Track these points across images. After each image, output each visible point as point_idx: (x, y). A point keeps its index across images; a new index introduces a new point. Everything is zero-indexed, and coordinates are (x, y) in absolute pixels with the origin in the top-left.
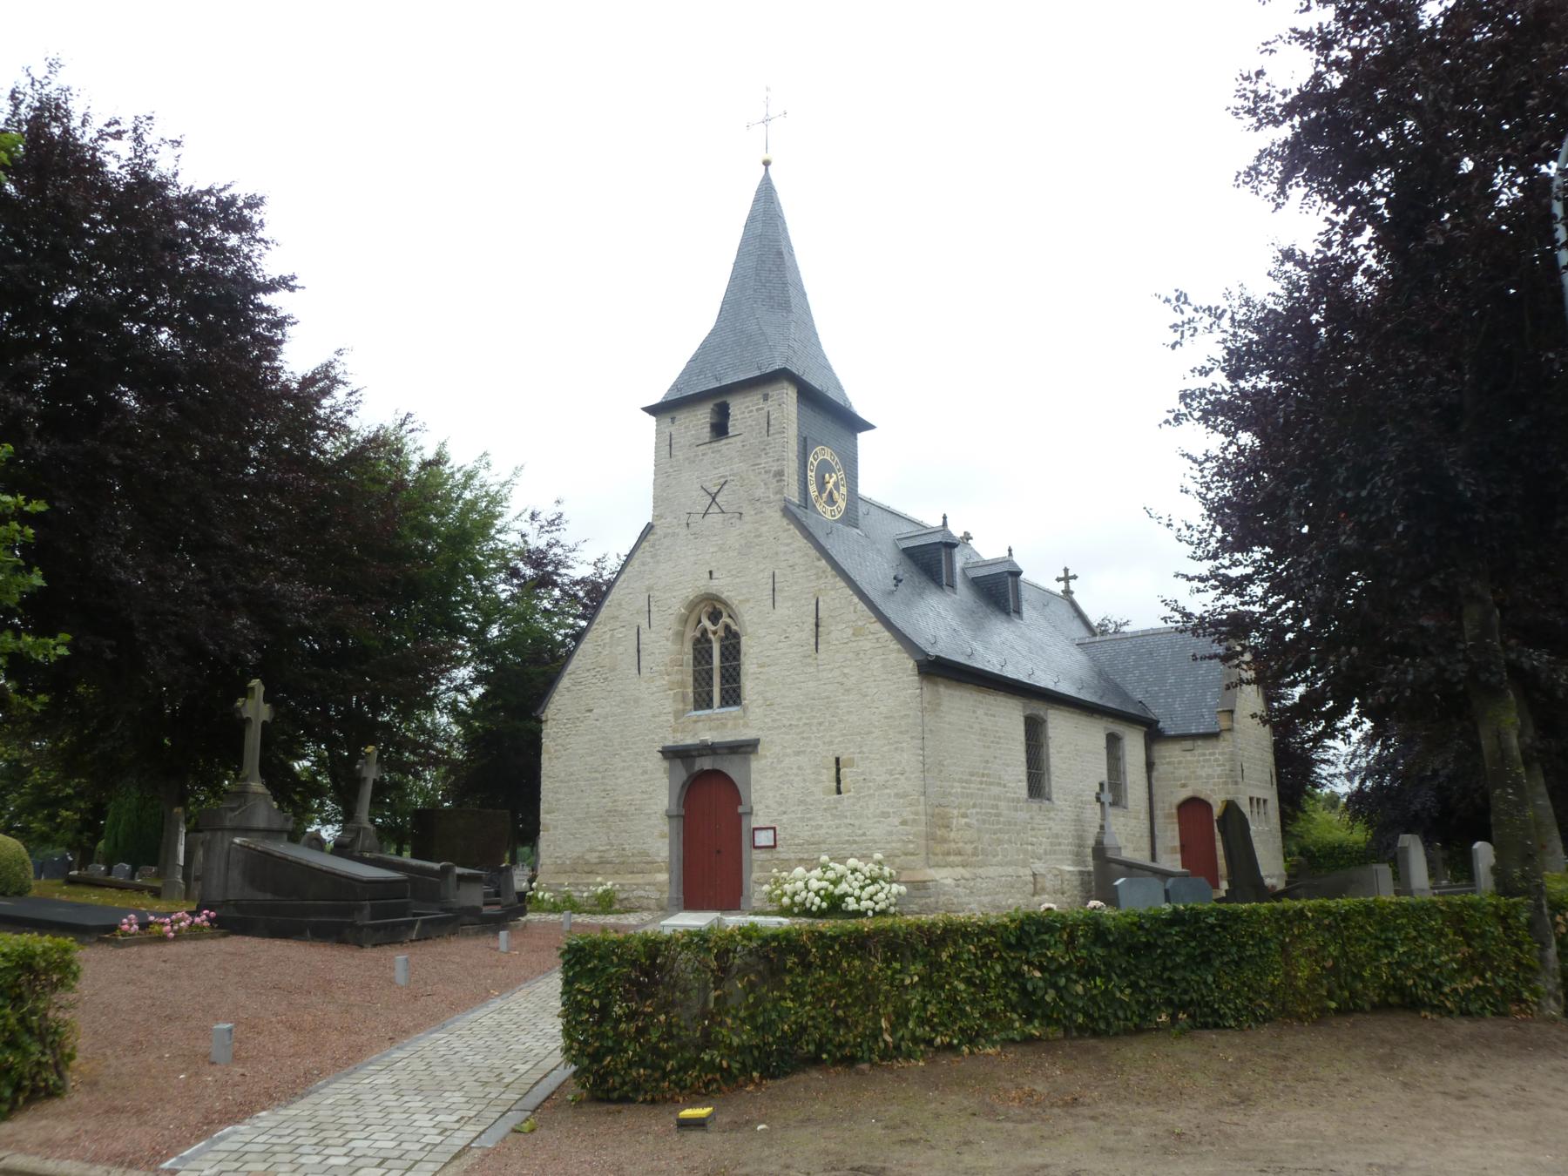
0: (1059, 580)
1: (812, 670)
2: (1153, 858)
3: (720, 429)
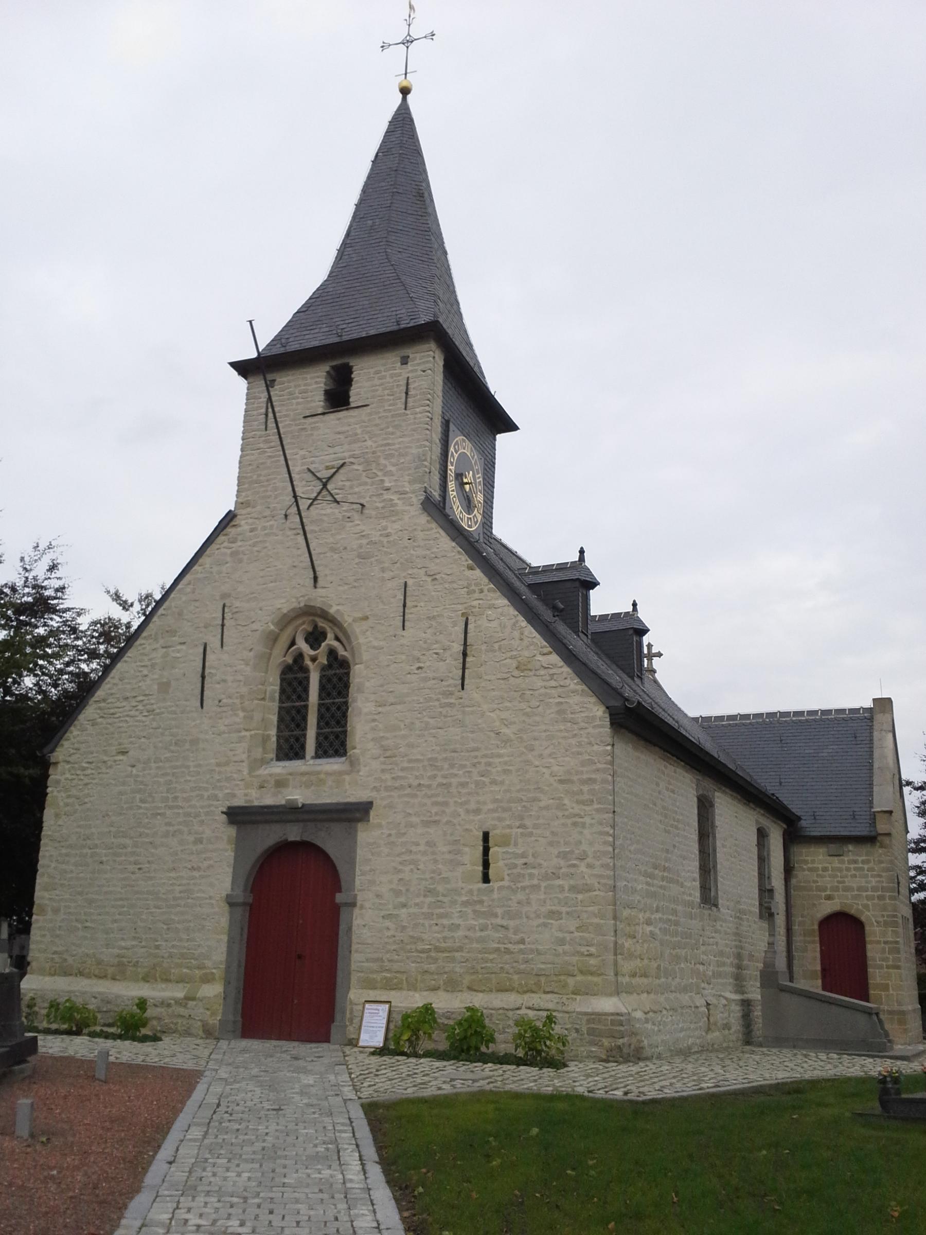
3: (338, 398)
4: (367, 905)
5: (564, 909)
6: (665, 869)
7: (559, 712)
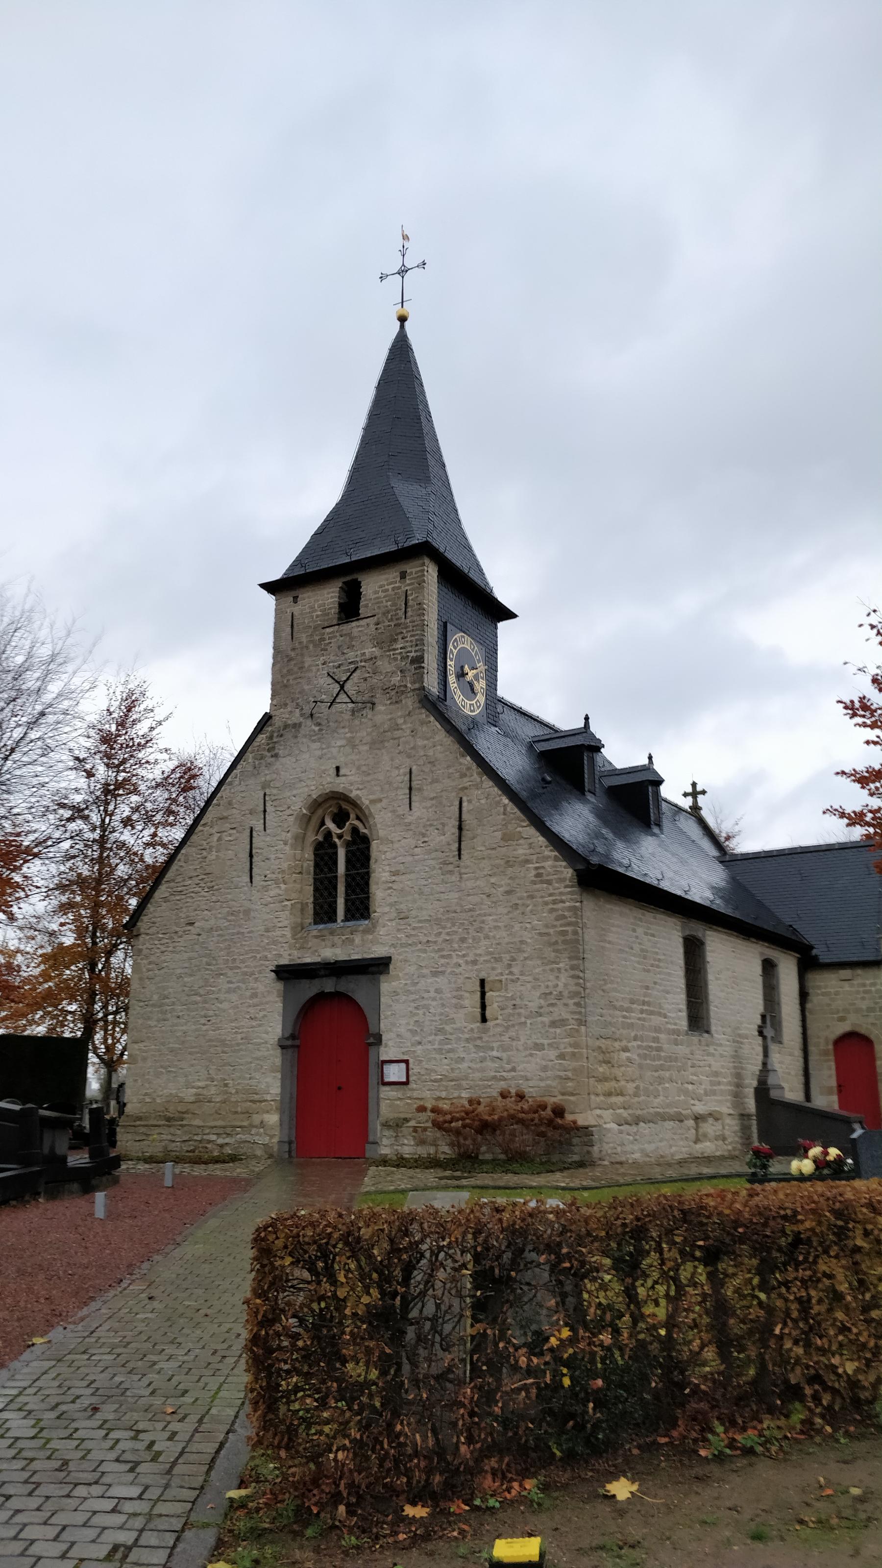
0: (685, 795)
1: (453, 878)
2: (808, 1097)
3: (349, 609)
4: (390, 1043)
5: (546, 1042)
6: (644, 1003)
7: (538, 875)
